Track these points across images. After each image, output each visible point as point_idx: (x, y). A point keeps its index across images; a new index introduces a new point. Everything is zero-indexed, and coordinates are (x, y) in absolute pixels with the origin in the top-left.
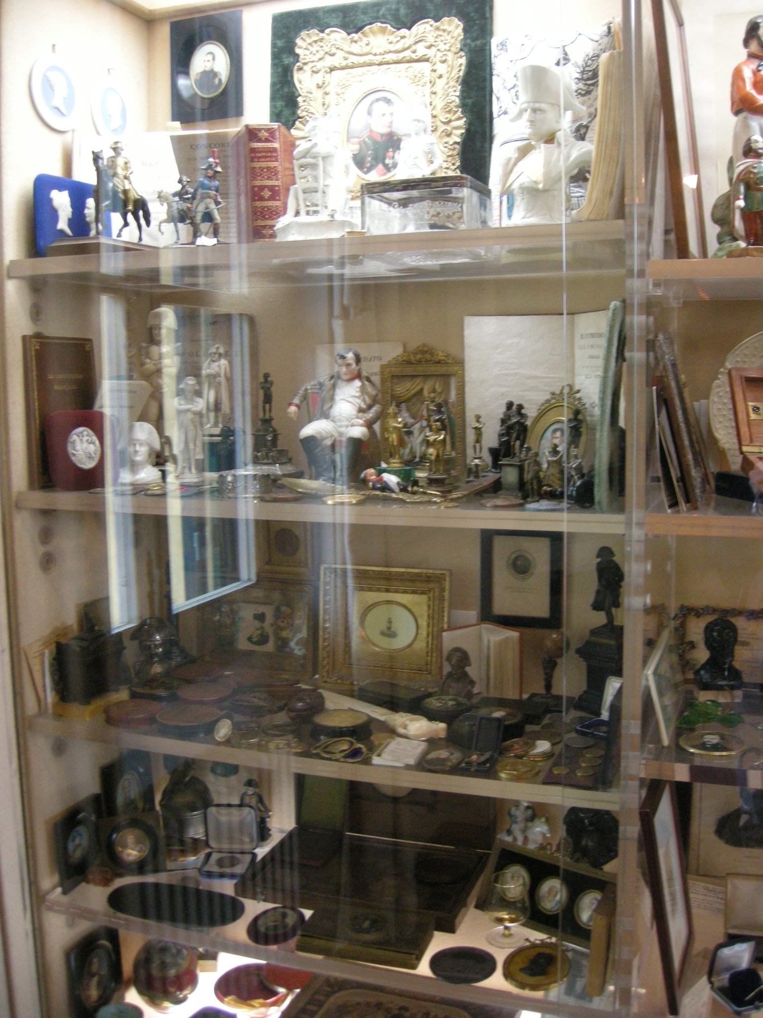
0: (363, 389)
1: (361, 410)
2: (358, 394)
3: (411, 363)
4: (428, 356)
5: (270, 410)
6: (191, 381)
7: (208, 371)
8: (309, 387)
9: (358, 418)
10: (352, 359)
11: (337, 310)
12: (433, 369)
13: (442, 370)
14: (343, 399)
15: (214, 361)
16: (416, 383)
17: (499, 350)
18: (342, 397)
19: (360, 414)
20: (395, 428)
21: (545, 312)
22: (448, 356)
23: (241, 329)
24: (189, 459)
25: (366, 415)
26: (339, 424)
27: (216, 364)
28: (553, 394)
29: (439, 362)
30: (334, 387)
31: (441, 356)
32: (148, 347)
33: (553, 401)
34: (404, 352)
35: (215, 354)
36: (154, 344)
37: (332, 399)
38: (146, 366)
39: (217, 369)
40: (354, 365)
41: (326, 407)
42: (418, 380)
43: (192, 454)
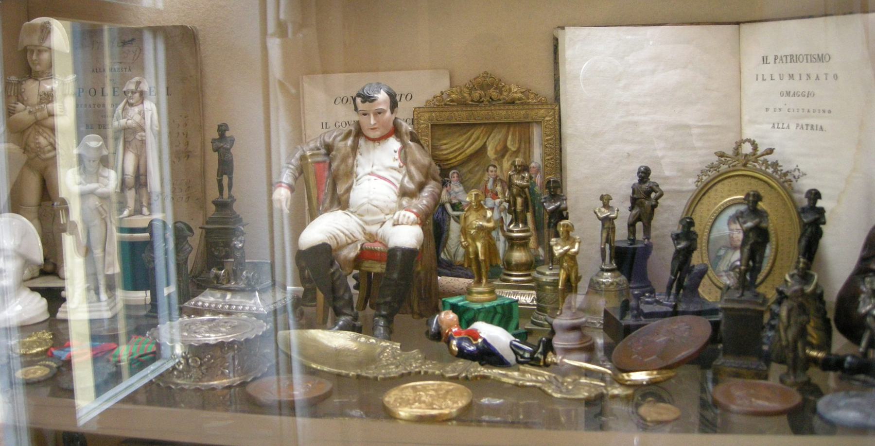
0: (404, 155)
1: (404, 193)
2: (396, 164)
3: (466, 105)
4: (494, 94)
5: (230, 186)
6: (94, 142)
7: (123, 122)
8: (308, 153)
9: (401, 207)
10: (385, 102)
11: (271, 26)
12: (502, 114)
13: (517, 114)
14: (371, 174)
15: (132, 105)
16: (474, 136)
17: (622, 84)
18: (368, 169)
19: (405, 201)
20: (481, 229)
21: (649, 23)
22: (527, 92)
23: (155, 49)
24: (95, 274)
25: (414, 201)
26: (368, 218)
27: (136, 109)
28: (721, 155)
29: (512, 102)
30: (355, 148)
31: (516, 92)
32: (20, 83)
33: (724, 168)
34: (451, 86)
35: (133, 92)
36: (30, 77)
37: (350, 174)
38: (17, 116)
39: (137, 118)
40: (388, 113)
41: (341, 189)
42: (477, 132)
43: (99, 266)
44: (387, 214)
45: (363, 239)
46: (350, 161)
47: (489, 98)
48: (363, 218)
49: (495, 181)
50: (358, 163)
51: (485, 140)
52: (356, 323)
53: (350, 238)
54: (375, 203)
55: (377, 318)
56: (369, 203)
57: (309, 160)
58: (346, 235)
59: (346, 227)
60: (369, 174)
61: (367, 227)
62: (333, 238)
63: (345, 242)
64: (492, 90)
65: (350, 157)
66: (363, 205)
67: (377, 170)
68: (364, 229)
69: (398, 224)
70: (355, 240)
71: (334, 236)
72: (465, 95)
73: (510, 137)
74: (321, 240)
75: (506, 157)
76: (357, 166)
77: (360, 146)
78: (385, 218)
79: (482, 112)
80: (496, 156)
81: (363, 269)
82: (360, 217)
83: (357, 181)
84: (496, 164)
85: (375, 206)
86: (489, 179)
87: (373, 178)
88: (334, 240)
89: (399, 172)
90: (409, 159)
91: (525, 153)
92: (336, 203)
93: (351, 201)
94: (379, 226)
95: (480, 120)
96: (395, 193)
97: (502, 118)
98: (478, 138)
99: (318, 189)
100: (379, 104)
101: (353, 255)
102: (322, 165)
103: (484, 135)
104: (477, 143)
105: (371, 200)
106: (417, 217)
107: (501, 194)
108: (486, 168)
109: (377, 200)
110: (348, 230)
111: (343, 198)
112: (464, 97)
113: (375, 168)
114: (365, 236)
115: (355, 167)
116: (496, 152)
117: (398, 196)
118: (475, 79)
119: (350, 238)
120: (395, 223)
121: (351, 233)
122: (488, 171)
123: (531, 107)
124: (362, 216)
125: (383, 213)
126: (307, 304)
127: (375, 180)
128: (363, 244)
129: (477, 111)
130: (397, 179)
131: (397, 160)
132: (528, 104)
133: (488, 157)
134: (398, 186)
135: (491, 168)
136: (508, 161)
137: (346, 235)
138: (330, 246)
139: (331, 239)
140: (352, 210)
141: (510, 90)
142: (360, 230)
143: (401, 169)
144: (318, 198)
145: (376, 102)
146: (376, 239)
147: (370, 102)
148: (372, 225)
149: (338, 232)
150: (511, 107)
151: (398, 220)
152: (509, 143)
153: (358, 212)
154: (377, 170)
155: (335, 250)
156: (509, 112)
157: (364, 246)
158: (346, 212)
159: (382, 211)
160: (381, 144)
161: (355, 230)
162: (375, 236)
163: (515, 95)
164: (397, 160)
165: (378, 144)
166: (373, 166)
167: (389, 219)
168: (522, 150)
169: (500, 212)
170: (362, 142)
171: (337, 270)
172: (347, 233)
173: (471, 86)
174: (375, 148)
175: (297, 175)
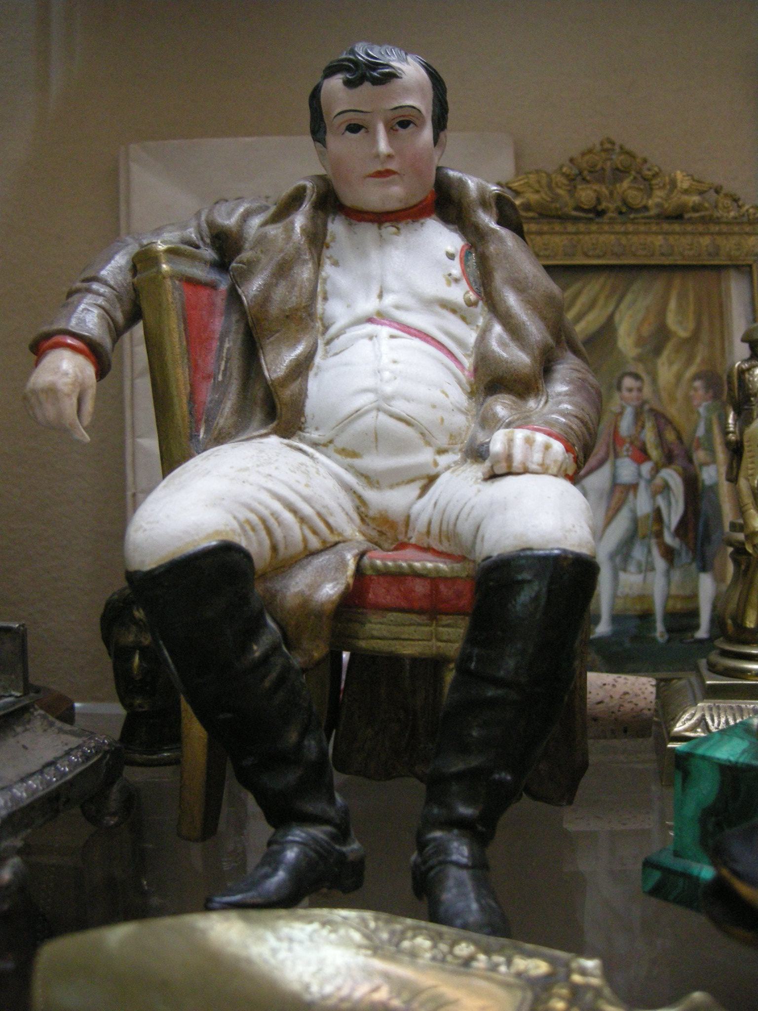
2: (459, 293)
14: (378, 318)
16: (583, 300)
18: (368, 305)
29: (677, 216)
44: (441, 452)
45: (359, 537)
46: (305, 273)
47: (619, 203)
48: (357, 462)
49: (638, 415)
50: (328, 287)
51: (610, 309)
52: (344, 849)
53: (315, 532)
54: (400, 407)
55: (438, 834)
56: (379, 409)
57: (165, 267)
58: (303, 520)
59: (301, 488)
60: (370, 320)
61: (371, 495)
62: (260, 527)
63: (301, 546)
64: (626, 184)
65: (305, 262)
66: (357, 414)
67: (397, 307)
68: (361, 504)
69: (509, 473)
70: (332, 539)
71: (264, 521)
72: (561, 192)
73: (673, 305)
74: (217, 533)
75: (666, 353)
76: (325, 299)
77: (334, 239)
78: (436, 464)
79: (602, 238)
80: (639, 350)
81: (363, 644)
82: (349, 460)
83: (328, 343)
84: (640, 369)
85: (400, 419)
86: (623, 408)
87: (384, 331)
88: (263, 533)
89: (464, 319)
90: (498, 277)
91: (711, 344)
92: (259, 416)
93: (311, 406)
94: (417, 492)
95: (599, 257)
96: (460, 383)
97: (652, 255)
98: (592, 305)
99: (194, 368)
100: (407, 91)
101: (330, 591)
102: (204, 293)
103: (608, 298)
104: (590, 317)
105: (388, 399)
106: (567, 451)
107: (657, 448)
108: (615, 382)
109: (408, 399)
110: (307, 500)
111: (286, 394)
112: (556, 198)
113: (389, 300)
114: (364, 528)
115: (320, 299)
116: (640, 341)
117: (471, 394)
118: (583, 154)
119: (315, 532)
120: (498, 471)
121: (319, 514)
122: (619, 388)
123: (724, 228)
124: (354, 455)
125: (428, 444)
126: (137, 757)
127: (392, 337)
128: (362, 555)
129: (589, 233)
130: (460, 343)
131: (457, 281)
132: (717, 221)
133: (620, 352)
134: (468, 363)
135: (628, 382)
136: (671, 363)
137: (303, 520)
138: (247, 555)
139: (253, 529)
140: (315, 435)
141: (673, 183)
142: (348, 504)
143: (472, 309)
144: (192, 399)
145: (395, 84)
146: (401, 537)
147: (376, 82)
148: (391, 487)
149: (277, 506)
150: (677, 227)
151: (509, 458)
152: (671, 320)
153: (340, 443)
154: (397, 307)
155: (264, 576)
156: (671, 239)
157: (366, 560)
158: (295, 443)
159: (426, 436)
160: (403, 231)
161: (333, 504)
162: (402, 528)
163: (685, 198)
164: (457, 281)
165: (394, 229)
166: (380, 296)
167: (448, 468)
168: (705, 337)
169: (653, 496)
170: (337, 227)
171: (274, 649)
172: (307, 510)
173: (575, 171)
174: (382, 242)
175: (119, 317)
